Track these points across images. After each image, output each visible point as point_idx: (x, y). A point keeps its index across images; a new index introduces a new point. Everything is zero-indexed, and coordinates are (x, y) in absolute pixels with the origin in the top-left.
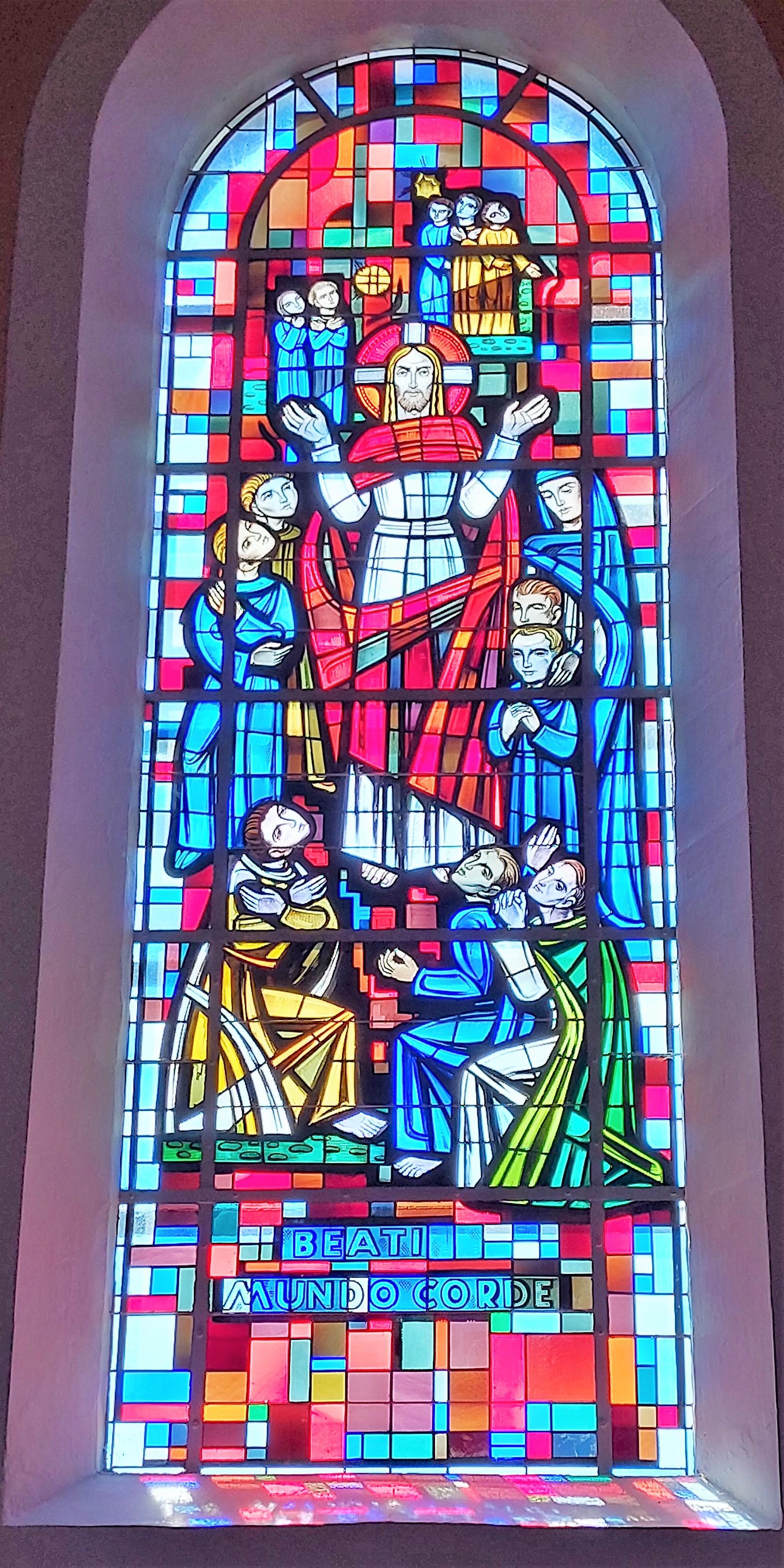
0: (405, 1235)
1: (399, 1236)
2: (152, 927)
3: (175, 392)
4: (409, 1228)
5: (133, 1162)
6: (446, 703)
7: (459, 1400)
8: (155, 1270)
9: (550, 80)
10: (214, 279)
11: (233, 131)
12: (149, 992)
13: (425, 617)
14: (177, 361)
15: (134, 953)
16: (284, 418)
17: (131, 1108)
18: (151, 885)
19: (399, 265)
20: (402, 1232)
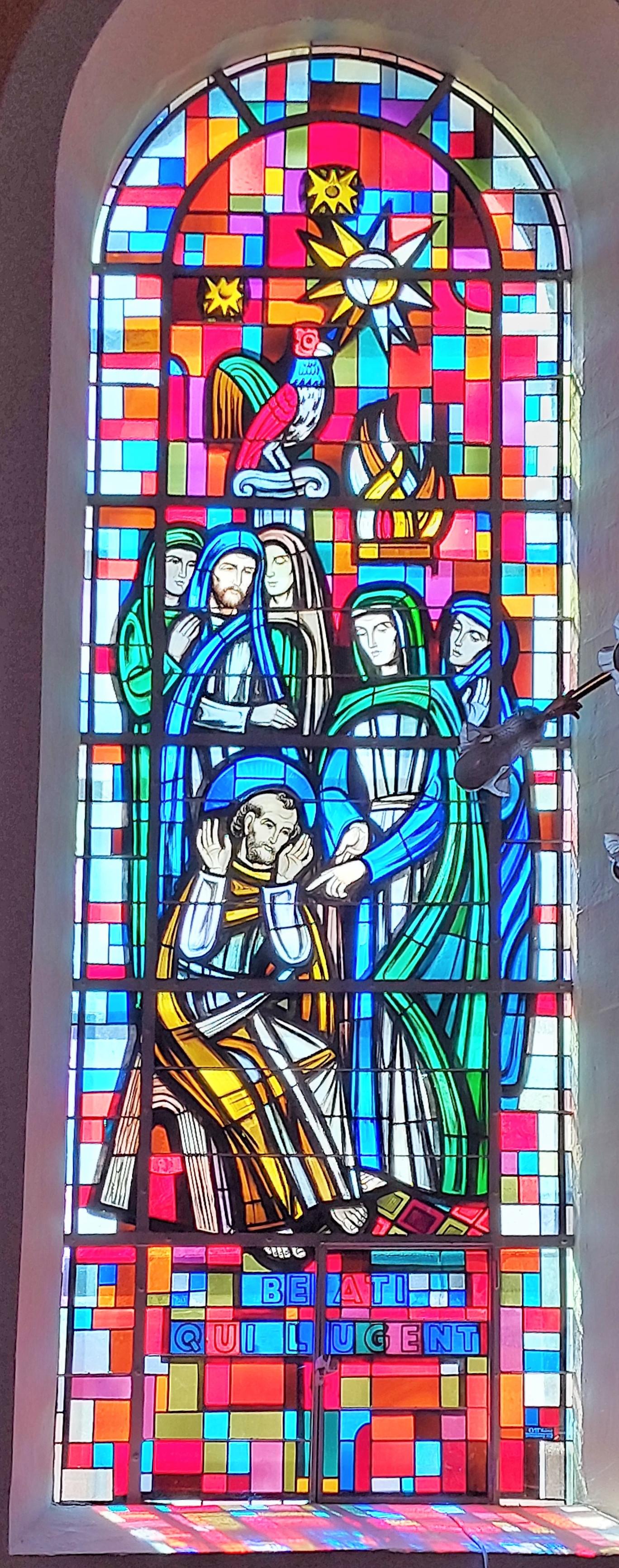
0: (388, 1283)
1: (382, 1283)
2: (97, 730)
3: (105, 356)
4: (392, 1277)
5: (71, 1330)
6: (440, 996)
7: (252, 192)
8: (97, 1402)
9: (400, 59)
10: (120, 580)
11: (134, 160)
12: (78, 1301)
13: (446, 1139)
14: (111, 234)
15: (75, 954)
16: (200, 830)
17: (62, 1410)
18: (93, 825)
19: (276, 287)
20: (385, 1279)
